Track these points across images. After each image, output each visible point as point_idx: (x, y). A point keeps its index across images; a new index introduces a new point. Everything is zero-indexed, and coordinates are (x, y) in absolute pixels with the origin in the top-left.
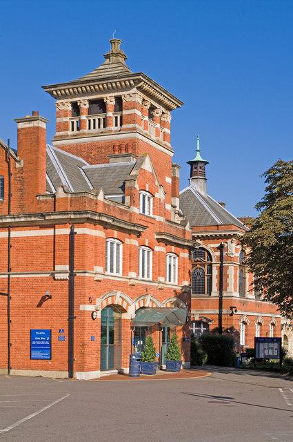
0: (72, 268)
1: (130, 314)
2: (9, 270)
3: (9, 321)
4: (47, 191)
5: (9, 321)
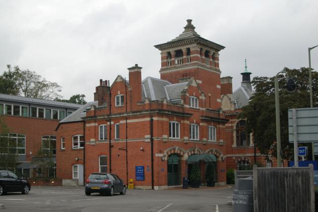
0: (152, 136)
1: (186, 157)
2: (127, 138)
3: (127, 163)
4: (138, 102)
5: (127, 163)
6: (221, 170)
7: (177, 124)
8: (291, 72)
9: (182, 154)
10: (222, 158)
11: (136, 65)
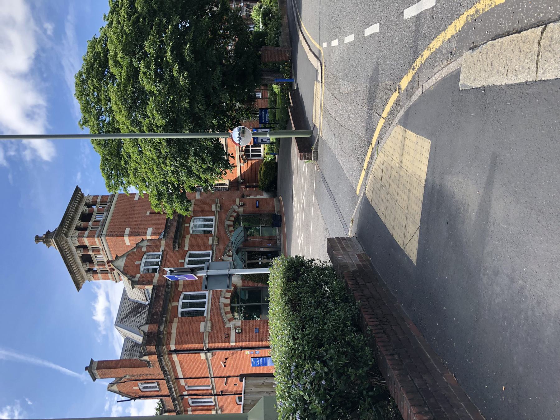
6: (257, 207)
7: (191, 256)
8: (104, 165)
9: (235, 214)
10: (240, 206)
11: (87, 368)
